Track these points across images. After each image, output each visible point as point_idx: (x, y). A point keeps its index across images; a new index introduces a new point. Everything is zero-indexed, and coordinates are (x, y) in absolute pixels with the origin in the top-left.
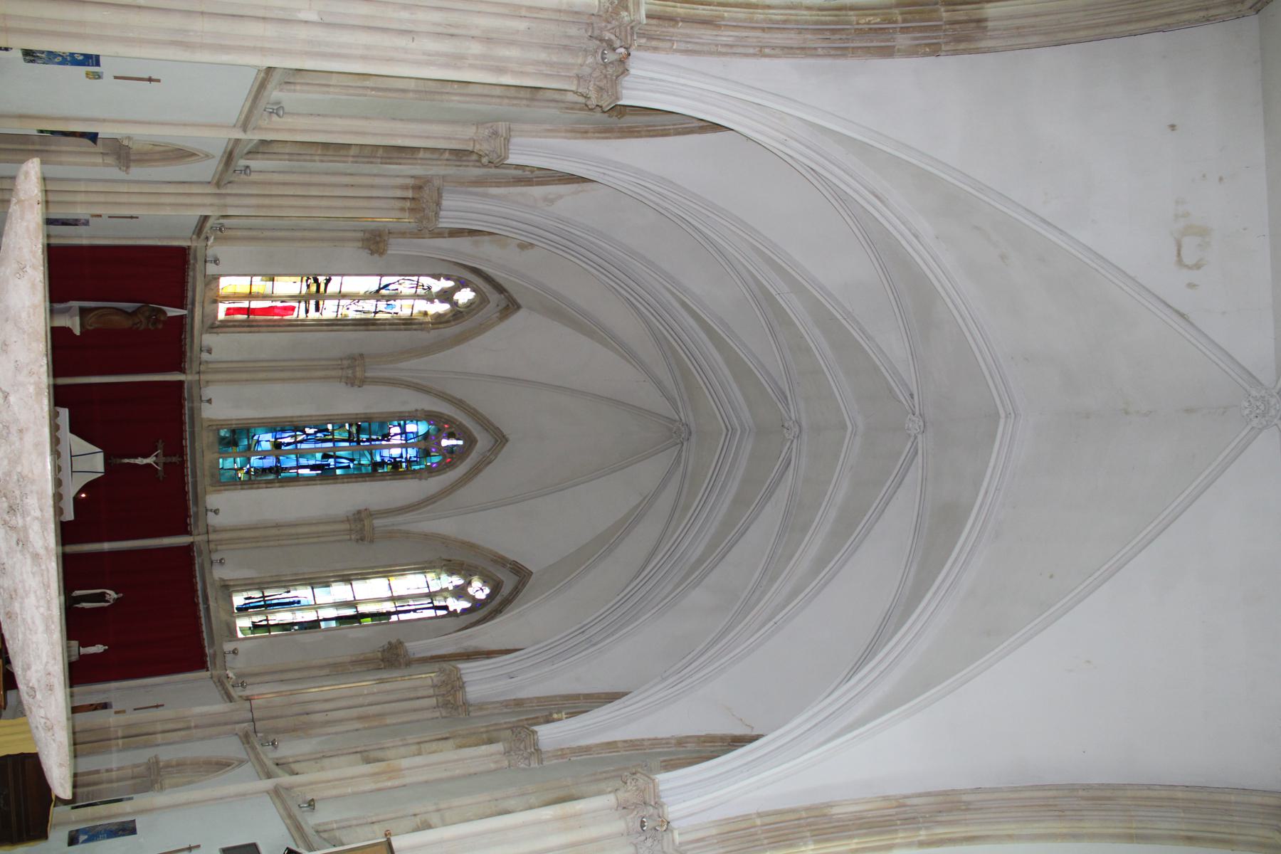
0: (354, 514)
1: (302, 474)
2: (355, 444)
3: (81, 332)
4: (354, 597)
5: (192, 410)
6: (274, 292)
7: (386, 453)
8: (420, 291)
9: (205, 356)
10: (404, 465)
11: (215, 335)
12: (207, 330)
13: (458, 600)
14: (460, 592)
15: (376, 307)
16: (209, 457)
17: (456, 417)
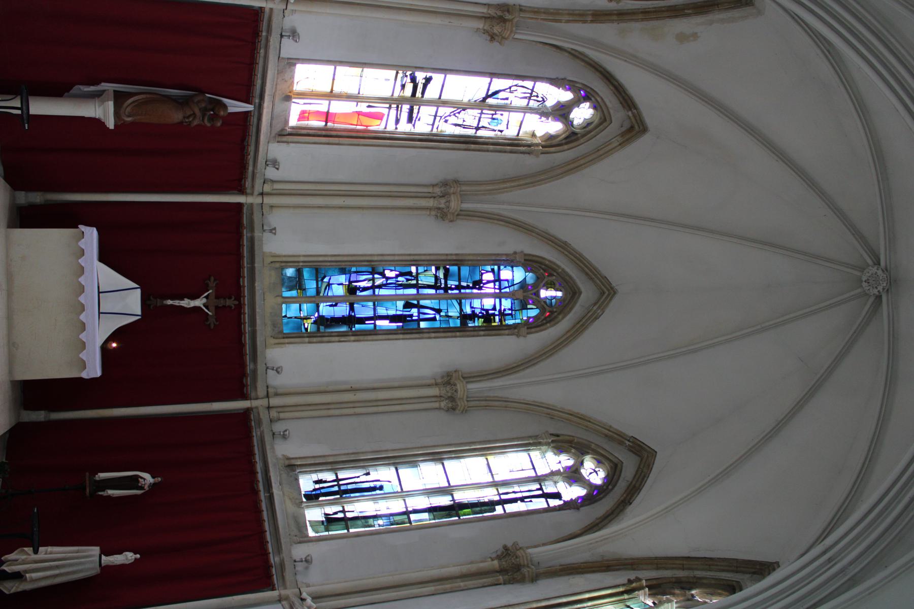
0: (443, 377)
1: (380, 326)
2: (442, 291)
3: (115, 126)
4: (448, 481)
5: (252, 240)
6: (361, 93)
7: (477, 303)
8: (533, 104)
9: (271, 173)
10: (497, 318)
11: (285, 144)
12: (275, 137)
13: (570, 486)
14: (573, 475)
15: (479, 121)
16: (271, 300)
17: (558, 262)
